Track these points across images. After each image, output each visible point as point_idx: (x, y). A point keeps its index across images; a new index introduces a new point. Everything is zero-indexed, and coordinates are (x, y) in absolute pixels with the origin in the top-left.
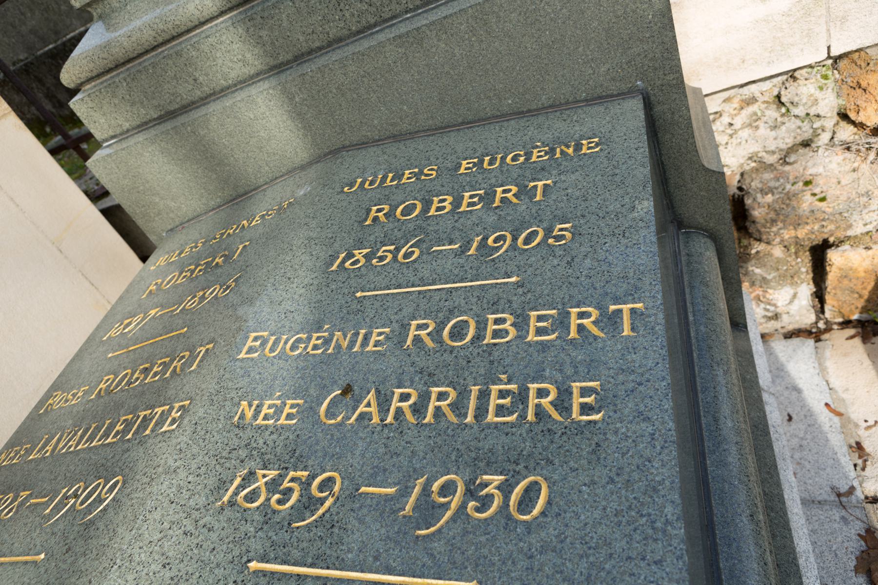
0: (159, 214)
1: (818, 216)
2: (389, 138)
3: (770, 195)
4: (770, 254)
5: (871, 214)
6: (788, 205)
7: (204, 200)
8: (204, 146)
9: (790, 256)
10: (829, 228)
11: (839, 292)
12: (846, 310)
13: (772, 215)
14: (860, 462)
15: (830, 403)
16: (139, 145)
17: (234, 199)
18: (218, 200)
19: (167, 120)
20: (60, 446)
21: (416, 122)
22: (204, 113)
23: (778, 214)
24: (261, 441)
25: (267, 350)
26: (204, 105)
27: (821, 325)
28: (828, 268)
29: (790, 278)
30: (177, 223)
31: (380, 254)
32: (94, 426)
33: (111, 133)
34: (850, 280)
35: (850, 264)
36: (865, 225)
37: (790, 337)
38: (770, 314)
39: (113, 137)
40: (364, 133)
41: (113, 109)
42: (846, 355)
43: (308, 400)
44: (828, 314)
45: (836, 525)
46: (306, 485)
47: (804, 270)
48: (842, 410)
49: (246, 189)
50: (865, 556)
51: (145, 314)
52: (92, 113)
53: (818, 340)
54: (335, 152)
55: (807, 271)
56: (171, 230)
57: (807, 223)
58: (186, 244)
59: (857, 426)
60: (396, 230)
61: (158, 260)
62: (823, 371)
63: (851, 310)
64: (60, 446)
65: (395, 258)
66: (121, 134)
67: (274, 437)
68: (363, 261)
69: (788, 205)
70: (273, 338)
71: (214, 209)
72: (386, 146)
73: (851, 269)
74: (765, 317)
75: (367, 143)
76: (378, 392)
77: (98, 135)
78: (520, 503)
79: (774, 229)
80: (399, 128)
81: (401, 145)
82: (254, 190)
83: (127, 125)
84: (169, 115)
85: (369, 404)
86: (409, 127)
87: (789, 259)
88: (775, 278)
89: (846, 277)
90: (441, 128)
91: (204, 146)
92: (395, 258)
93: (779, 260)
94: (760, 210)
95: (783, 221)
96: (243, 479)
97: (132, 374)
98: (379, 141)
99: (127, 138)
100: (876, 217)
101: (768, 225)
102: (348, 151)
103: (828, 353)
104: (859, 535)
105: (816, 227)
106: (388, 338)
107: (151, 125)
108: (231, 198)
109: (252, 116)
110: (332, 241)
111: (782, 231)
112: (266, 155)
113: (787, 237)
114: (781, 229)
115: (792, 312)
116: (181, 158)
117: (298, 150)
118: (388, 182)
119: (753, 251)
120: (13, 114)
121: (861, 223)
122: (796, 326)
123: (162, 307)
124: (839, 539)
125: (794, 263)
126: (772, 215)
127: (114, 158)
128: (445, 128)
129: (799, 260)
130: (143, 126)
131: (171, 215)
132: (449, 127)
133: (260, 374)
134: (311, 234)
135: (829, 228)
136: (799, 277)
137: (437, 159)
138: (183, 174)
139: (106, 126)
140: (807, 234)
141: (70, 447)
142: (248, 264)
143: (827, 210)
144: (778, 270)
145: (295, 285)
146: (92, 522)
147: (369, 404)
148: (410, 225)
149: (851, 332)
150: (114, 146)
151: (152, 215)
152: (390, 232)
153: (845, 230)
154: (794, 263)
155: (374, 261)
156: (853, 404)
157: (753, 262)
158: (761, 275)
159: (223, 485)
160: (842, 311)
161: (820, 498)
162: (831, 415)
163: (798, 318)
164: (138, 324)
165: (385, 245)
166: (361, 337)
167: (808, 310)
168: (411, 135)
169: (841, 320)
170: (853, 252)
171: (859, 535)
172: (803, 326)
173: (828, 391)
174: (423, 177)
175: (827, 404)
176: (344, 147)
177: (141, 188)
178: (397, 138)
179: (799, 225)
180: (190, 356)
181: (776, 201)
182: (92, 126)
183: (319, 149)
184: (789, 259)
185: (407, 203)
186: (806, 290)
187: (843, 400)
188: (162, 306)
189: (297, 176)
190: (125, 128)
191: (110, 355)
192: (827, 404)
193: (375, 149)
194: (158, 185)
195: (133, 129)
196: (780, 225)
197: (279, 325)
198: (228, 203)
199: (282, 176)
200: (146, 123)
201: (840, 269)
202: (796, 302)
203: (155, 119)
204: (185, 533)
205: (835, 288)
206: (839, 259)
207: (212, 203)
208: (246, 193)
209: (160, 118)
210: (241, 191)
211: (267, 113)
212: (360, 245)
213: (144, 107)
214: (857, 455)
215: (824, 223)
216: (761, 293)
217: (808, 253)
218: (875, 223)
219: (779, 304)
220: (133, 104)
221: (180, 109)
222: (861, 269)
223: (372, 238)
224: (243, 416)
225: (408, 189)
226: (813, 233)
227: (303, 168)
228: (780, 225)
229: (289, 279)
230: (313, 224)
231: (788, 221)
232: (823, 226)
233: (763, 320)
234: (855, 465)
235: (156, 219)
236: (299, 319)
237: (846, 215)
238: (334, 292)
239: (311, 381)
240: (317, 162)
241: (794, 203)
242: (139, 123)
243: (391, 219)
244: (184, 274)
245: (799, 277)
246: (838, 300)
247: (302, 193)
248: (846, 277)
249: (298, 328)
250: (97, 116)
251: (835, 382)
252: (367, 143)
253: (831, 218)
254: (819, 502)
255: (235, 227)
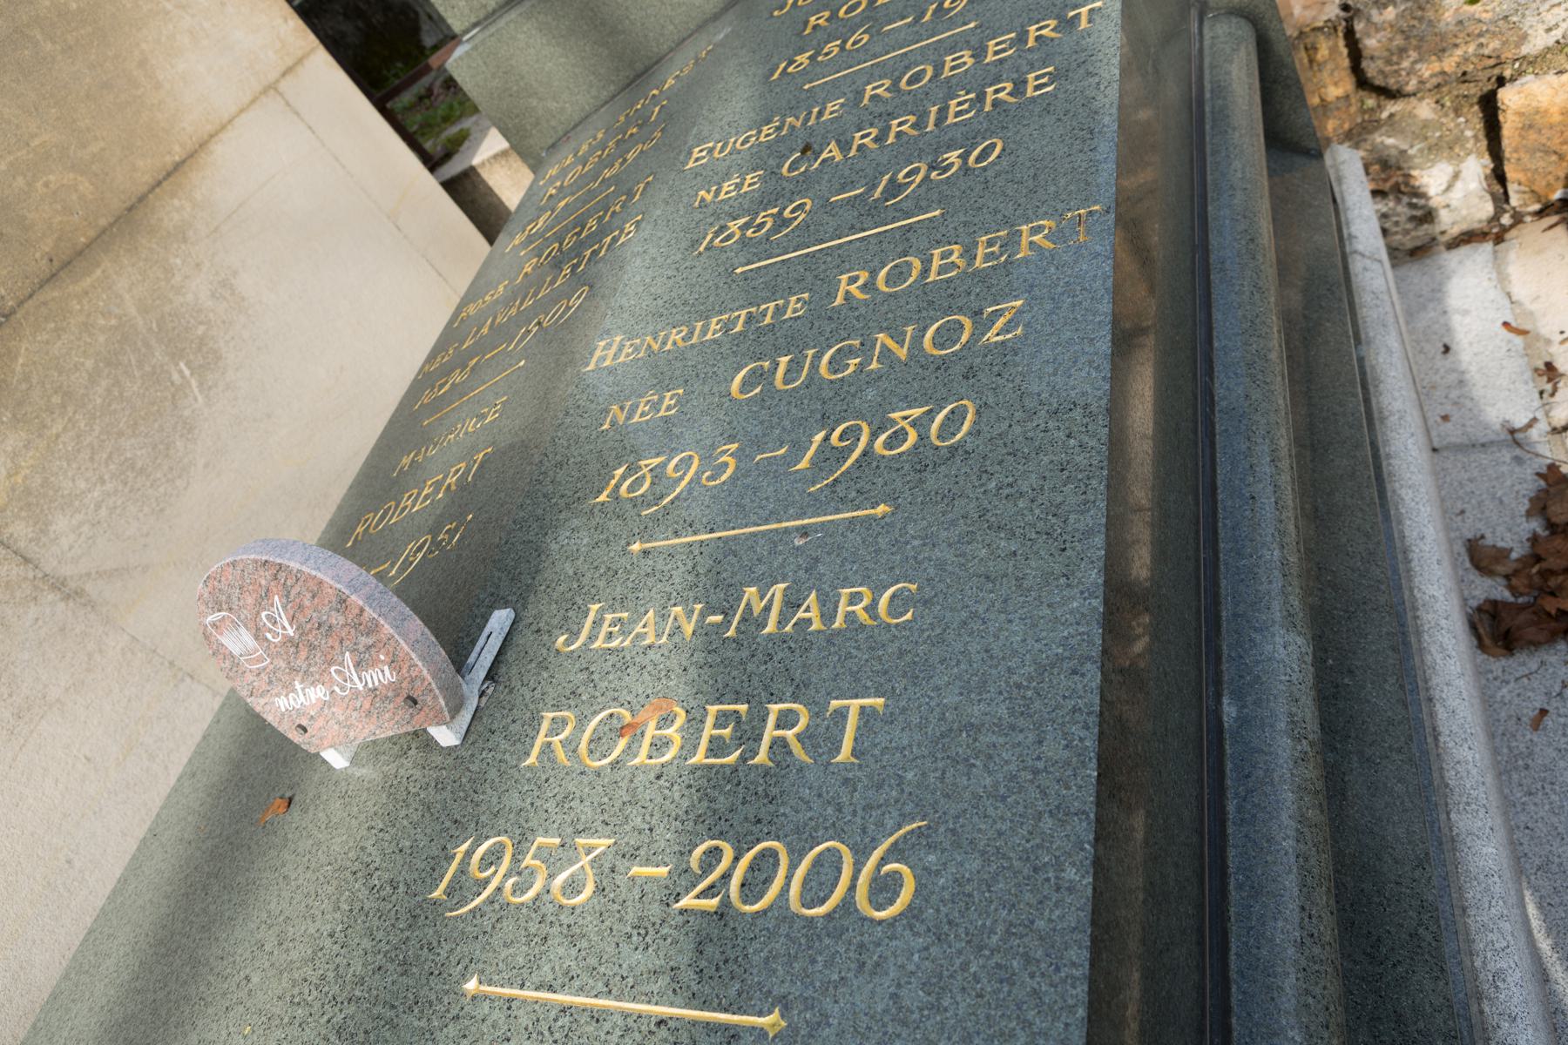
1: (1470, 30)
3: (1390, 8)
4: (1411, 115)
5: (1556, 10)
6: (1421, 19)
7: (594, 92)
9: (1446, 115)
10: (1491, 46)
11: (1526, 158)
12: (1540, 186)
13: (1399, 41)
14: (1549, 387)
15: (1509, 319)
23: (1407, 38)
27: (1506, 220)
28: (1501, 118)
29: (1446, 147)
33: (473, 20)
34: (1540, 131)
35: (1534, 104)
36: (1549, 30)
37: (1458, 246)
38: (1419, 213)
39: (475, 25)
42: (1540, 252)
44: (1515, 201)
45: (1505, 468)
47: (1469, 133)
48: (1527, 327)
50: (1542, 495)
53: (1499, 239)
55: (1475, 137)
56: (553, 146)
57: (1456, 46)
59: (1548, 342)
61: (512, 241)
62: (1502, 279)
63: (1549, 185)
66: (486, 18)
69: (1421, 19)
73: (1537, 112)
74: (1412, 218)
76: (838, 142)
79: (1406, 64)
82: (657, 62)
85: (832, 151)
87: (1444, 120)
88: (1421, 151)
89: (1530, 126)
93: (1426, 125)
94: (1379, 36)
95: (1418, 48)
100: (1564, 14)
101: (1395, 59)
103: (1512, 255)
104: (1538, 474)
105: (1471, 49)
111: (1418, 66)
113: (1427, 74)
114: (1415, 62)
115: (1454, 203)
119: (1385, 115)
121: (1541, 28)
122: (1464, 227)
124: (1508, 483)
125: (1452, 125)
126: (1399, 41)
129: (1462, 119)
131: (553, 123)
135: (1491, 46)
136: (1462, 146)
139: (467, 11)
140: (1458, 64)
143: (1484, 15)
144: (1426, 138)
147: (832, 151)
149: (1554, 219)
153: (1518, 45)
154: (1452, 125)
156: (1544, 315)
157: (1384, 129)
158: (1395, 147)
160: (1535, 188)
161: (1483, 440)
162: (1511, 336)
163: (1464, 212)
167: (1481, 198)
169: (1537, 207)
170: (1538, 83)
171: (1538, 474)
172: (1476, 226)
173: (1508, 305)
175: (1506, 324)
179: (1444, 50)
181: (1401, 16)
184: (1444, 120)
186: (1476, 167)
187: (1532, 313)
190: (490, 9)
192: (1506, 324)
196: (1414, 55)
201: (1521, 114)
202: (1459, 185)
205: (1516, 150)
206: (1516, 98)
207: (605, 94)
210: (639, 66)
212: (802, 51)
214: (1545, 378)
215: (1482, 40)
216: (1401, 179)
217: (1476, 108)
218: (1564, 26)
219: (1432, 192)
222: (1554, 110)
226: (1466, 60)
228: (1414, 55)
231: (1425, 47)
232: (1481, 45)
233: (1409, 226)
234: (1541, 393)
237: (1515, 19)
241: (1430, 14)
245: (1462, 146)
246: (1525, 170)
248: (1530, 126)
251: (1519, 292)
253: (1492, 28)
254: (1483, 445)
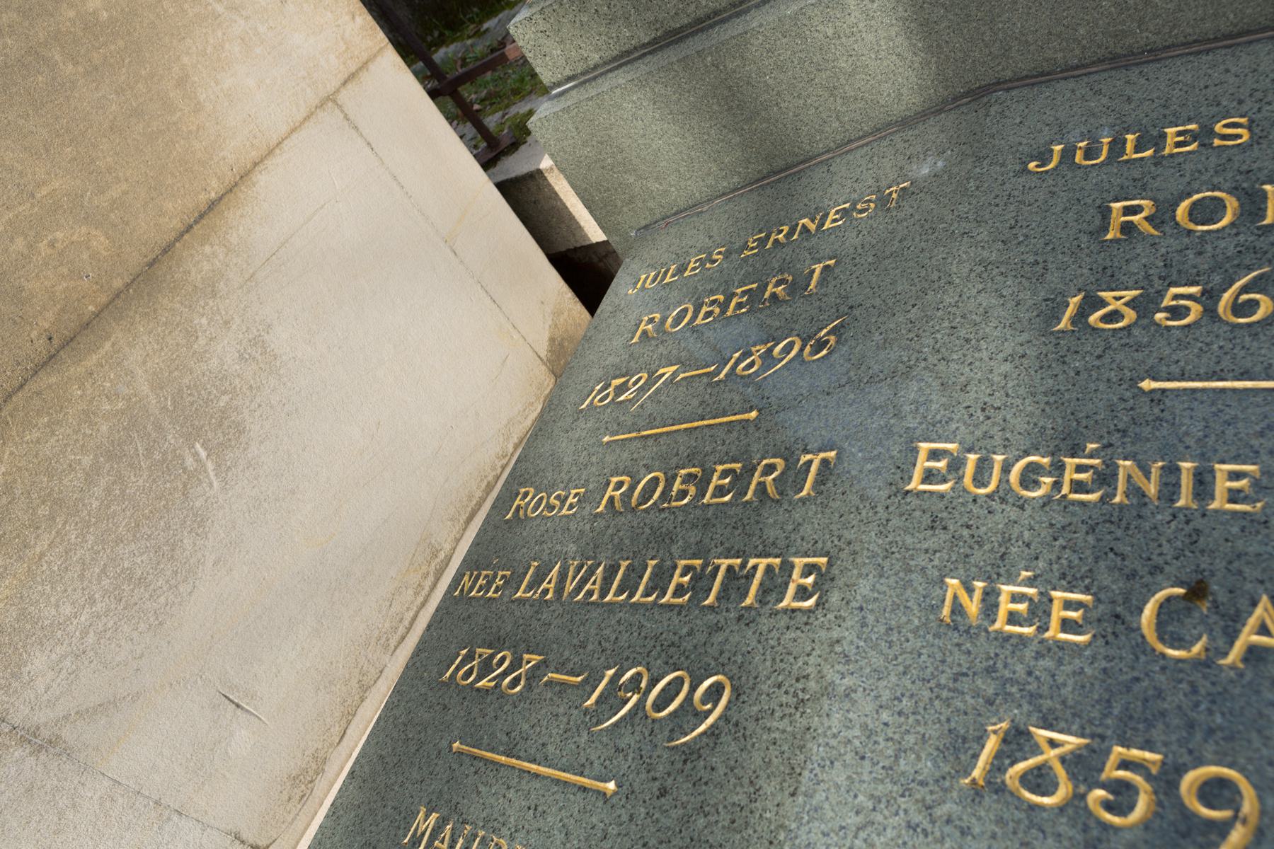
0: (631, 202)
2: (1100, 61)
7: (710, 181)
8: (730, 88)
16: (618, 91)
17: (764, 178)
18: (736, 179)
19: (668, 45)
20: (570, 587)
21: (1174, 26)
22: (740, 30)
24: (1020, 668)
25: (968, 480)
26: (738, 15)
30: (658, 216)
31: (1167, 302)
32: (624, 564)
33: (568, 72)
39: (569, 79)
40: (1049, 54)
41: (577, 32)
43: (1102, 596)
46: (1166, 781)
49: (789, 160)
51: (651, 374)
52: (543, 41)
54: (978, 94)
56: (646, 227)
58: (687, 253)
60: (1190, 254)
64: (570, 587)
65: (1210, 312)
66: (583, 74)
67: (1047, 663)
68: (1130, 316)
70: (972, 457)
71: (724, 194)
72: (1096, 77)
75: (1048, 74)
77: (546, 76)
78: (657, 485)
80: (1129, 41)
81: (1134, 74)
83: (595, 58)
84: (670, 38)
86: (1153, 38)
90: (1230, 36)
91: (730, 88)
92: (1210, 312)
96: (1004, 741)
97: (670, 482)
98: (1077, 67)
99: (595, 78)
102: (1008, 90)
106: (1256, 484)
107: (636, 55)
108: (759, 176)
109: (830, 32)
110: (1039, 268)
112: (839, 101)
116: (685, 109)
117: (904, 91)
118: (1130, 153)
120: (390, 46)
123: (684, 365)
127: (573, 113)
128: (1240, 35)
130: (624, 59)
131: (651, 204)
132: (1249, 32)
133: (968, 527)
134: (985, 254)
137: (1240, 102)
138: (684, 137)
139: (561, 61)
141: (590, 593)
142: (850, 302)
145: (985, 355)
146: (691, 753)
148: (1222, 244)
150: (574, 93)
151: (619, 204)
152: (1177, 257)
155: (1159, 316)
159: (961, 747)
164: (642, 390)
165: (1177, 285)
166: (1186, 482)
168: (1153, 54)
174: (1217, 142)
176: (998, 83)
177: (609, 161)
178: (1117, 61)
180: (787, 468)
182: (539, 62)
183: (946, 88)
185: (1196, 197)
188: (679, 361)
189: (897, 138)
190: (591, 63)
191: (606, 439)
193: (1071, 84)
194: (638, 156)
195: (606, 63)
197: (978, 433)
198: (752, 184)
199: (860, 138)
200: (628, 53)
203: (644, 46)
204: (909, 826)
208: (788, 168)
209: (654, 41)
211: (861, 25)
213: (629, 26)
220: (612, 21)
221: (690, 25)
223: (1134, 267)
224: (958, 609)
225: (1188, 167)
227: (905, 123)
229: (968, 341)
230: (983, 234)
235: (625, 209)
236: (1020, 424)
238: (1084, 375)
239: (1097, 559)
240: (940, 111)
242: (615, 53)
243: (1167, 229)
244: (705, 309)
247: (925, 171)
249: (1025, 443)
250: (550, 45)
252: (1048, 74)
255: (786, 229)
